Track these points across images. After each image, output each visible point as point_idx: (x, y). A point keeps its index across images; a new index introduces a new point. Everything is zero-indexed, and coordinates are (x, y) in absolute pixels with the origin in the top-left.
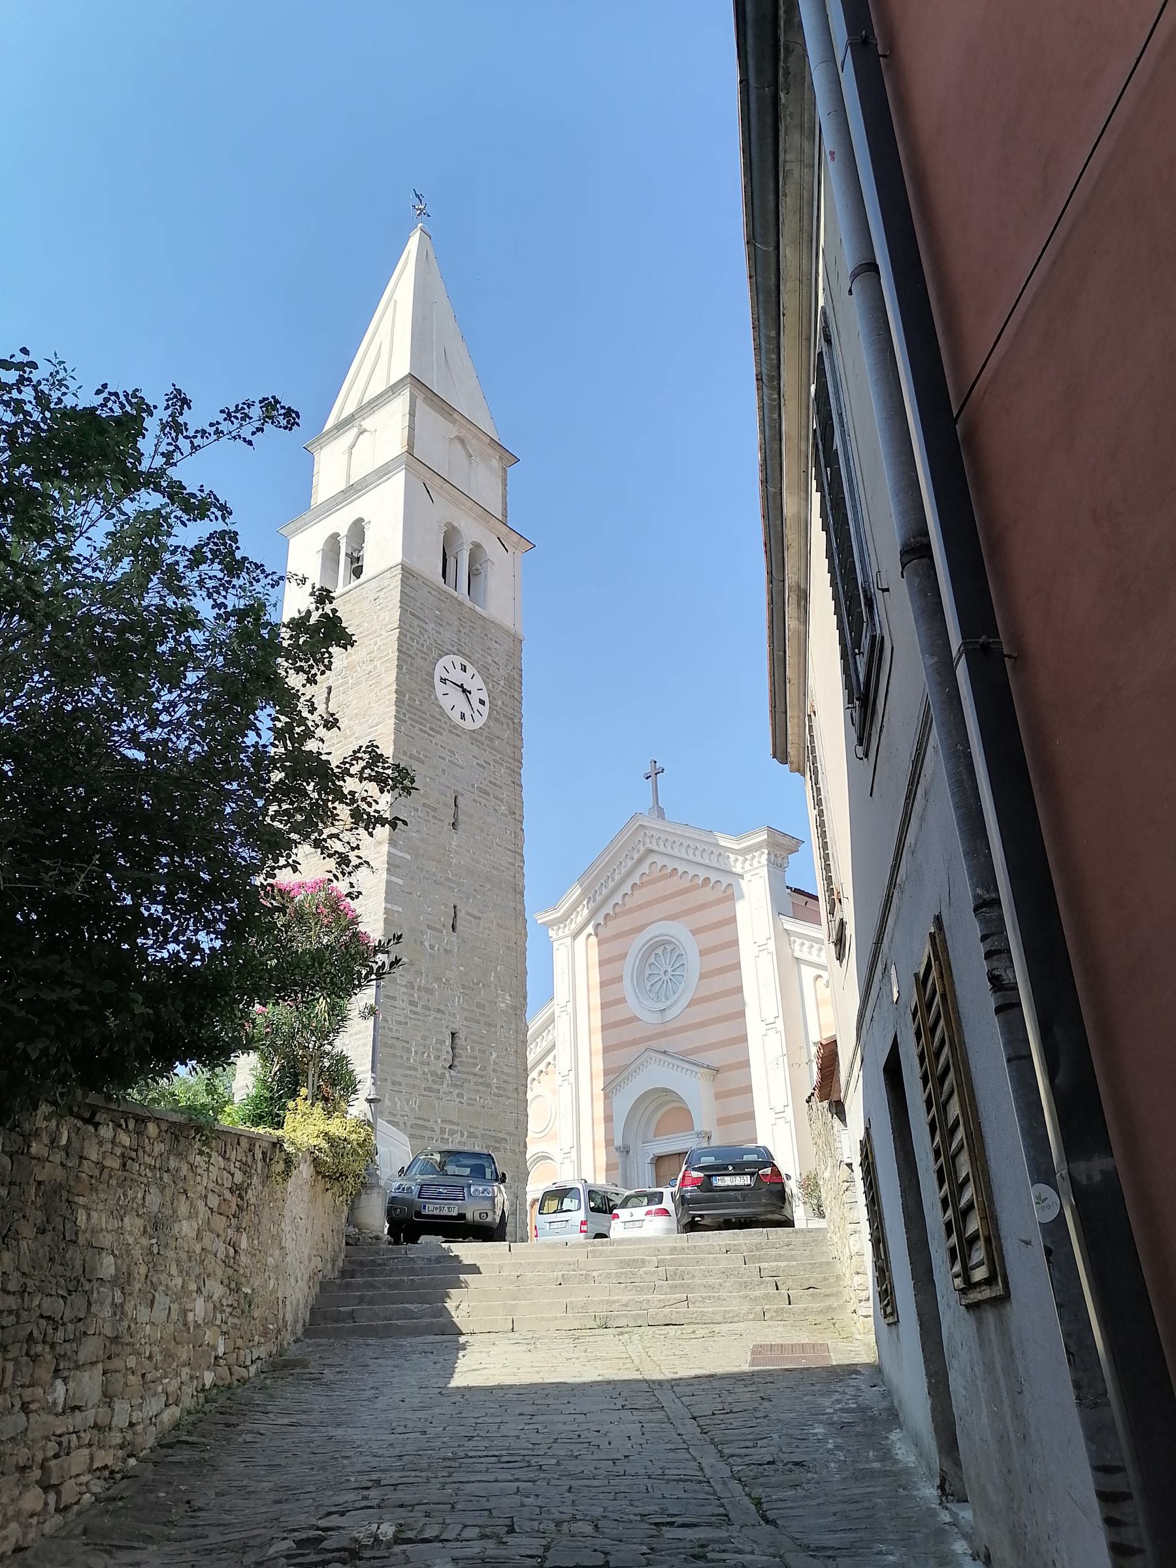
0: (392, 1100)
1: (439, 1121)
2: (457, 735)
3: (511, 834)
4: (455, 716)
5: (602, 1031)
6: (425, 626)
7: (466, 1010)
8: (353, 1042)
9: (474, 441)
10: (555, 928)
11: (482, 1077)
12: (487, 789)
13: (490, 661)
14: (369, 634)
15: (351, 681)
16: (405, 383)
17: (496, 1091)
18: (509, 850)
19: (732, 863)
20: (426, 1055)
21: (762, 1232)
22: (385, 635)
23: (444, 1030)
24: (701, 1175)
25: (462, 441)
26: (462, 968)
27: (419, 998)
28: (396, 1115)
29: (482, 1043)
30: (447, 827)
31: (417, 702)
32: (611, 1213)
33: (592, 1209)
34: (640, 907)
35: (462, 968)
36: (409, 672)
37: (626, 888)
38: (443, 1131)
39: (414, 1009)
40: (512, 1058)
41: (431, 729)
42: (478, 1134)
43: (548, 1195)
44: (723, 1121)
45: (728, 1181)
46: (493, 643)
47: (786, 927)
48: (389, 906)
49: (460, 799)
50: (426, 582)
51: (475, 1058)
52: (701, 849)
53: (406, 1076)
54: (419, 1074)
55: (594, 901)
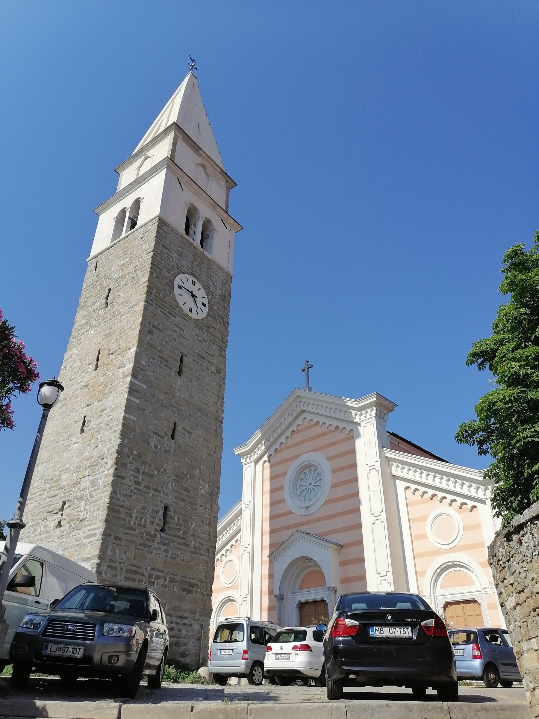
0: (113, 550)
1: (149, 569)
2: (186, 320)
3: (217, 385)
4: (186, 309)
5: (270, 520)
6: (171, 254)
7: (176, 492)
8: (91, 508)
9: (211, 169)
10: (245, 457)
11: (184, 539)
12: (203, 355)
13: (211, 284)
14: (136, 257)
15: (122, 284)
16: (172, 128)
17: (193, 550)
18: (214, 394)
19: (353, 416)
20: (143, 520)
21: (442, 707)
22: (144, 255)
23: (159, 503)
24: (356, 623)
25: (204, 167)
26: (176, 464)
27: (142, 479)
28: (115, 562)
29: (186, 516)
30: (173, 373)
31: (161, 296)
32: (266, 644)
33: (254, 641)
34: (295, 445)
35: (176, 464)
36: (157, 277)
37: (288, 433)
38: (150, 576)
39: (138, 487)
40: (207, 528)
41: (169, 313)
42: (178, 580)
43: (221, 628)
44: (345, 581)
45: (386, 632)
46: (214, 274)
47: (387, 455)
48: (127, 416)
49: (185, 358)
50: (174, 231)
51: (180, 525)
52: (334, 409)
53: (126, 534)
54: (136, 533)
55: (269, 441)
